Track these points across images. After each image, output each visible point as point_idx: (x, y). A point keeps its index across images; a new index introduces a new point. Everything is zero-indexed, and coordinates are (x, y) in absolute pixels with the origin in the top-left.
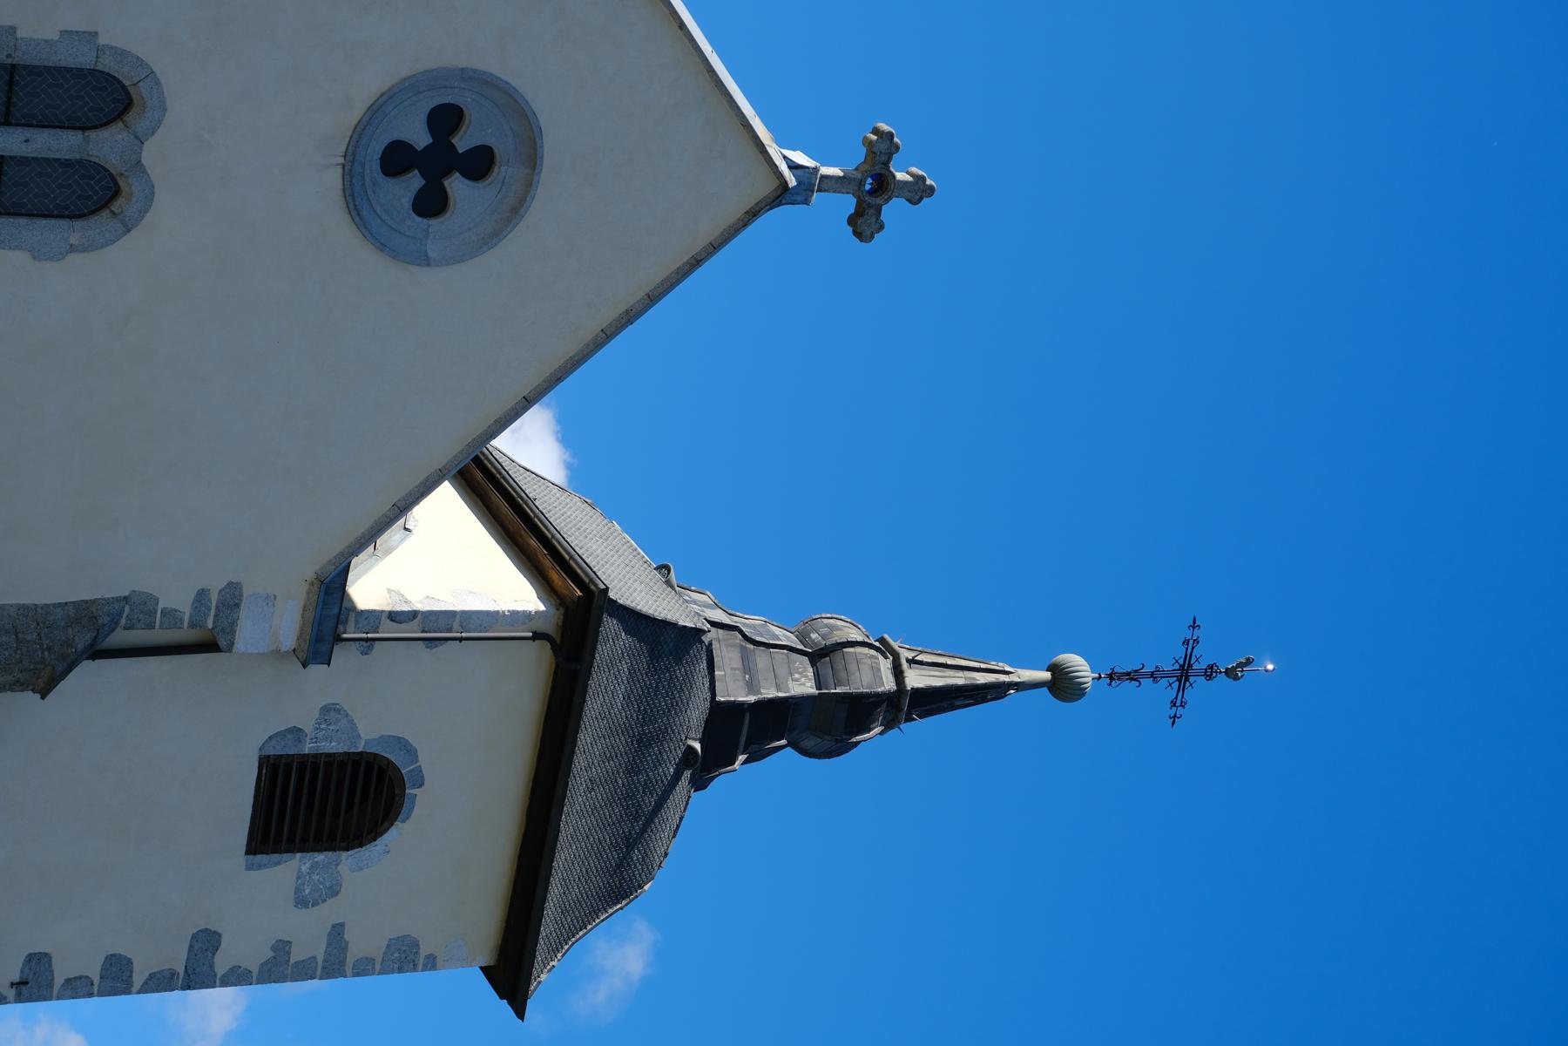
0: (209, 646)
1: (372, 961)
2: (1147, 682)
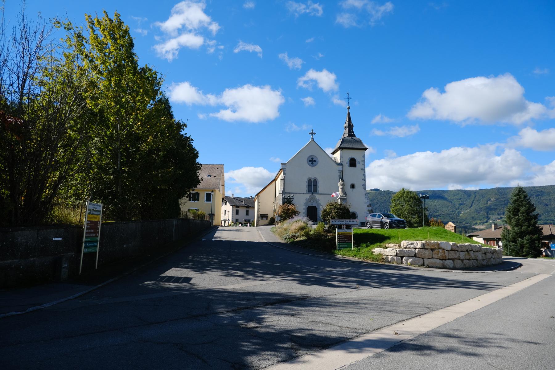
0: (342, 171)
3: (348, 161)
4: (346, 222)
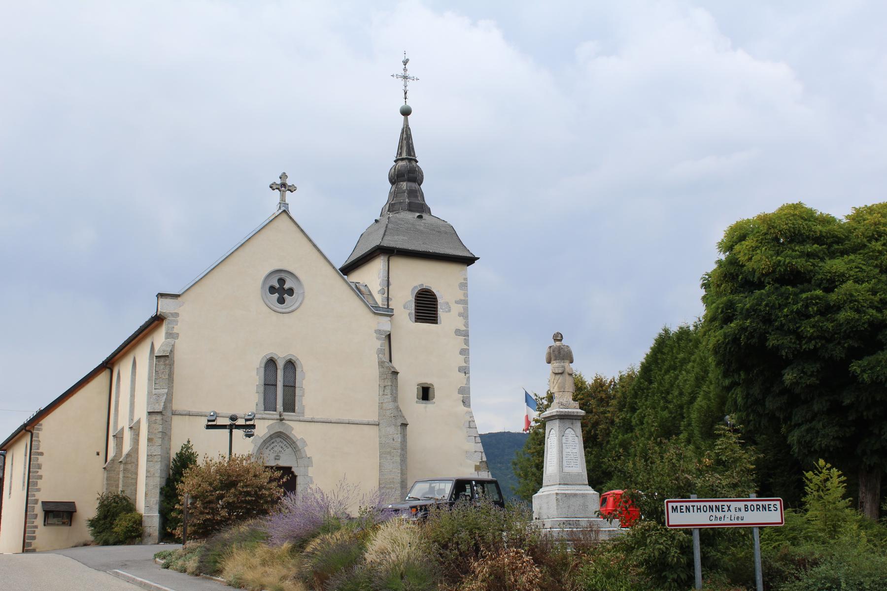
0: (389, 336)
1: (464, 293)
3: (411, 299)
4: (733, 513)
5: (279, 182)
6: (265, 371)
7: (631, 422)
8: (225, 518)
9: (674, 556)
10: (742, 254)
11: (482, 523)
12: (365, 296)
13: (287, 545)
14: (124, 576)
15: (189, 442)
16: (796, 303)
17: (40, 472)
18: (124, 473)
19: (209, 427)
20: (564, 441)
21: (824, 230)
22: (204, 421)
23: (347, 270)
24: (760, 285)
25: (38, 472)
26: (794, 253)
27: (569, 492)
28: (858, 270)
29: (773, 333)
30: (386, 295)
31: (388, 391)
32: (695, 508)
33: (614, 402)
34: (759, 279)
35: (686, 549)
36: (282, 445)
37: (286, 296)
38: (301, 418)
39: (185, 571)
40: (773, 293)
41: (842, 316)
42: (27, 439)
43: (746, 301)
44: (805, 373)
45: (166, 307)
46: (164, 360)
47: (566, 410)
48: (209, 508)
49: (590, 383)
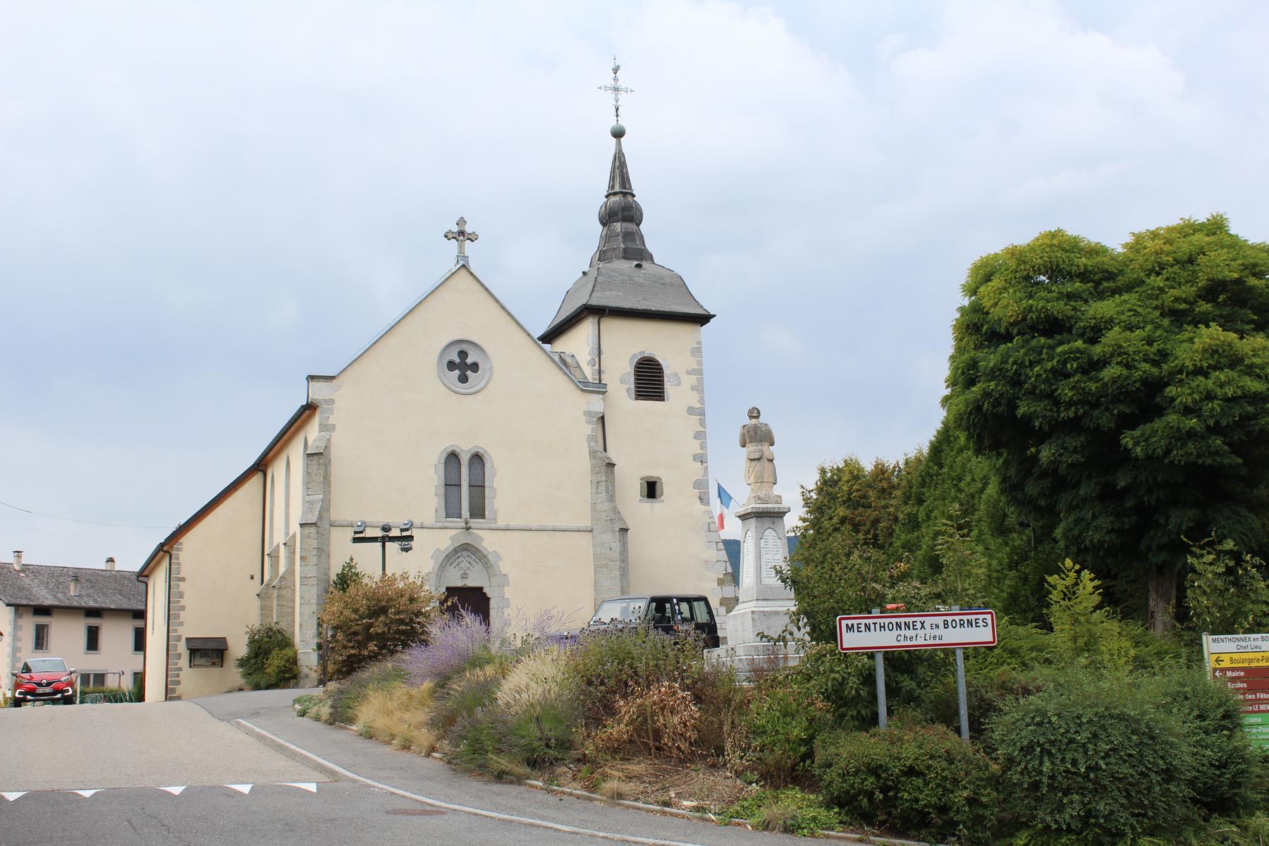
0: (603, 418)
1: (698, 361)
2: (619, 103)
4: (928, 630)
5: (455, 229)
6: (446, 468)
7: (918, 518)
8: (374, 652)
9: (852, 688)
10: (986, 299)
11: (636, 652)
12: (571, 369)
13: (427, 685)
14: (245, 726)
15: (352, 559)
16: (1051, 359)
17: (183, 602)
18: (278, 600)
19: (356, 540)
20: (763, 545)
21: (1090, 264)
22: (350, 534)
23: (550, 337)
24: (1008, 337)
25: (179, 602)
26: (1049, 295)
27: (769, 609)
28: (1131, 313)
29: (1024, 398)
30: (597, 367)
31: (602, 488)
32: (878, 626)
33: (898, 493)
34: (1007, 329)
35: (868, 679)
36: (469, 560)
37: (469, 373)
38: (493, 526)
39: (320, 720)
40: (1023, 347)
41: (1110, 372)
42: (166, 562)
43: (990, 359)
44: (1065, 449)
45: (319, 392)
46: (318, 458)
47: (765, 506)
48: (355, 641)
49: (869, 470)
